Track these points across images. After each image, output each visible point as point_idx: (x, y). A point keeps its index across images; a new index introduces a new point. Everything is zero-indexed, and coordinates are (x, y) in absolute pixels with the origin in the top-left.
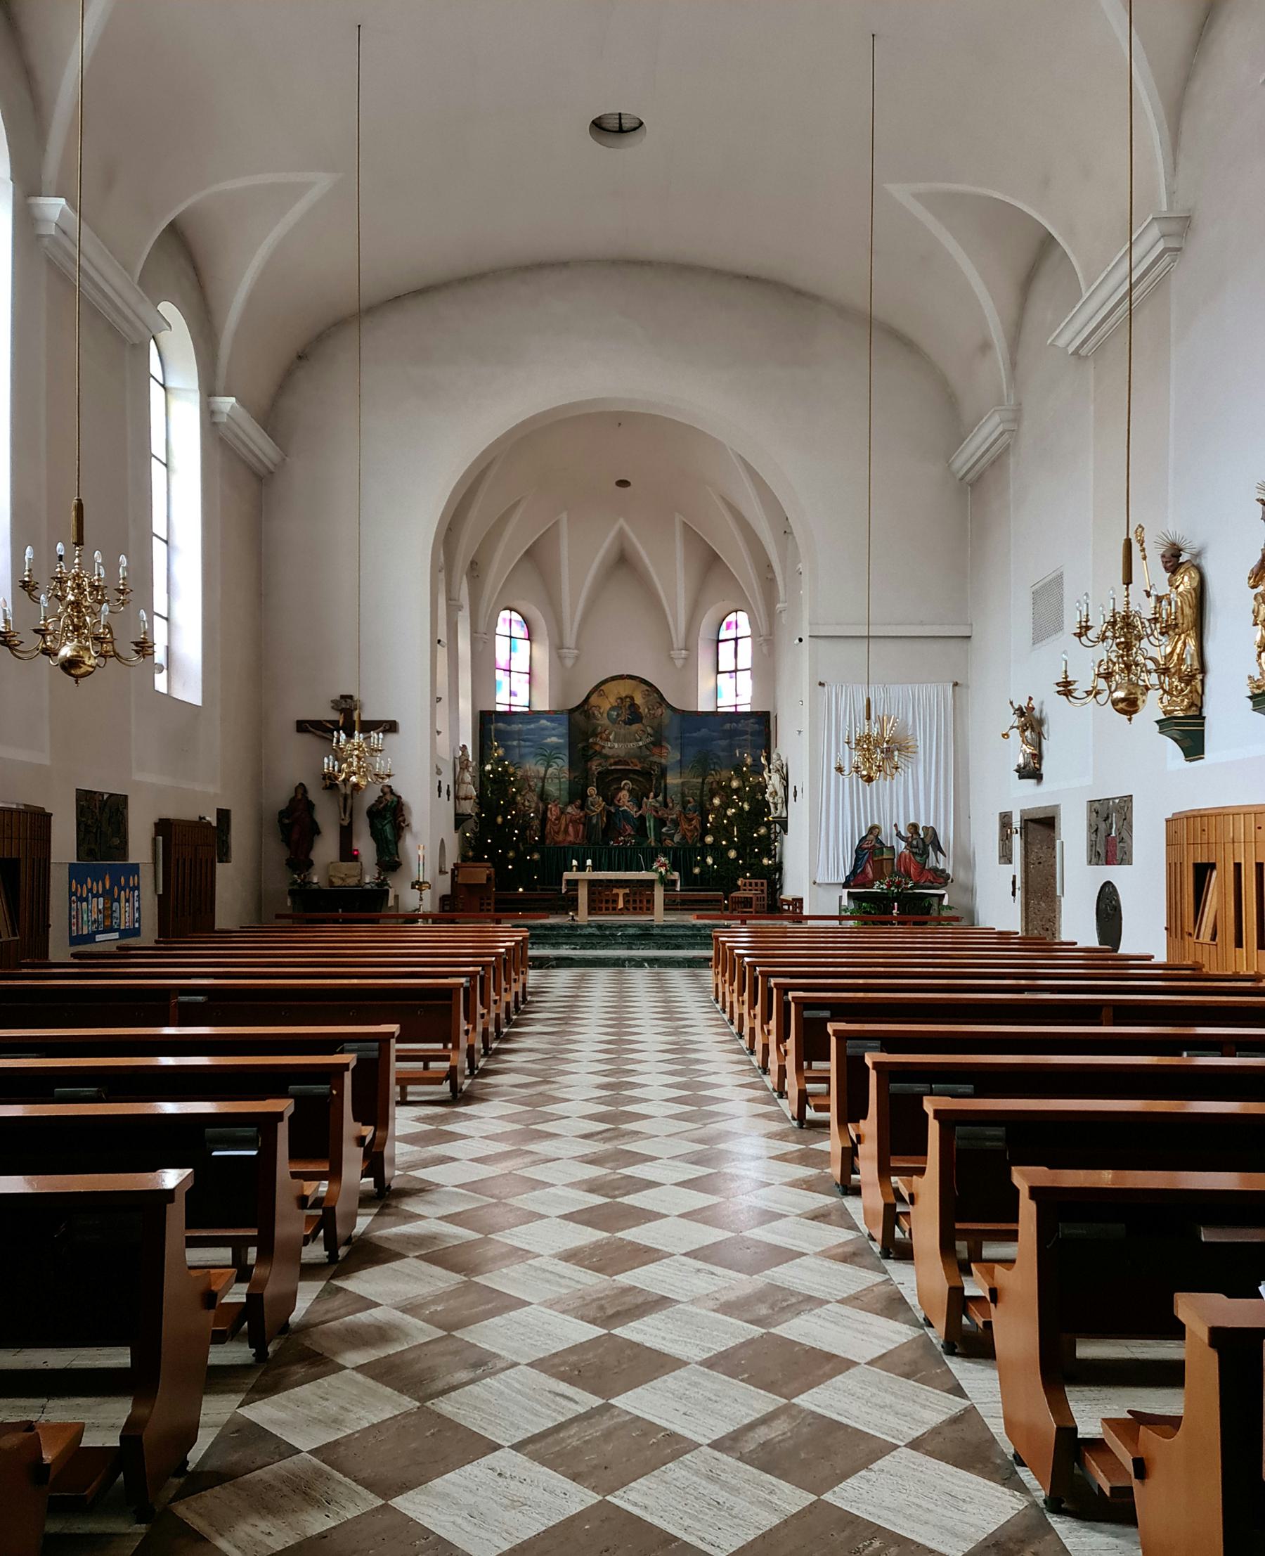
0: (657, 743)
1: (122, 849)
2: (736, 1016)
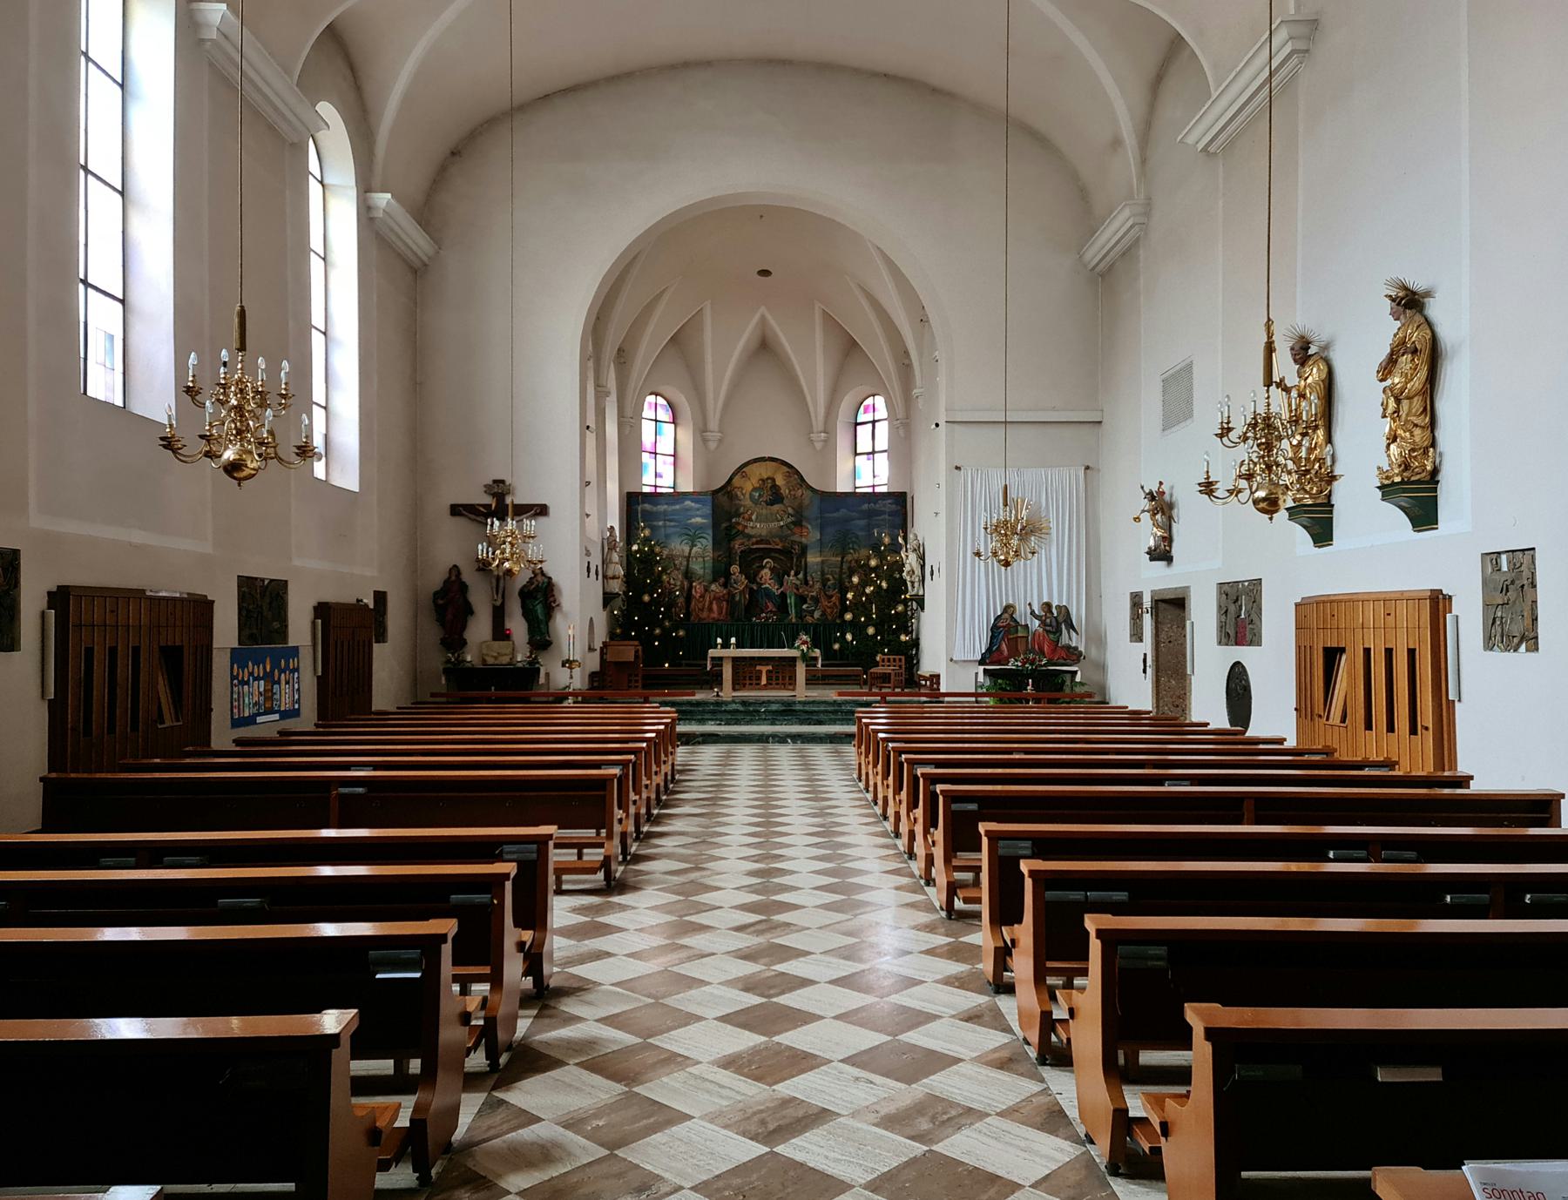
0: (798, 523)
1: (283, 633)
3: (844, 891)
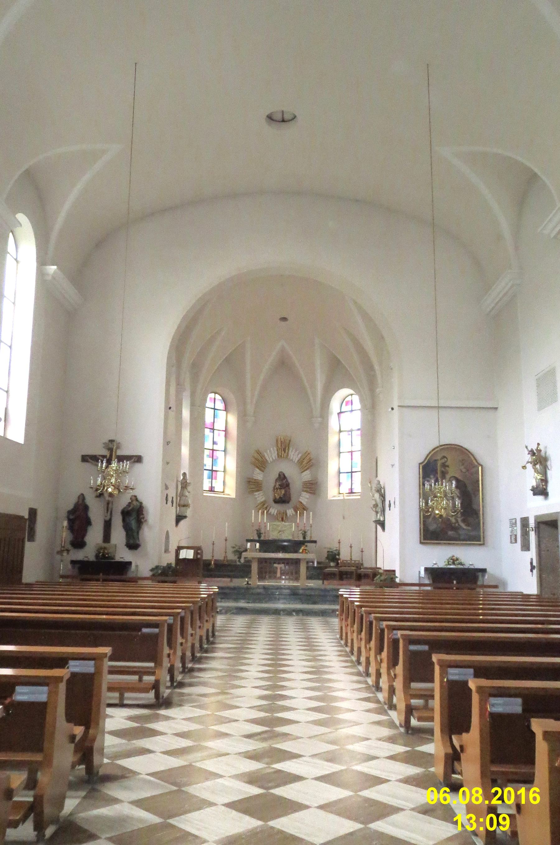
2: (355, 649)
3: (326, 710)
